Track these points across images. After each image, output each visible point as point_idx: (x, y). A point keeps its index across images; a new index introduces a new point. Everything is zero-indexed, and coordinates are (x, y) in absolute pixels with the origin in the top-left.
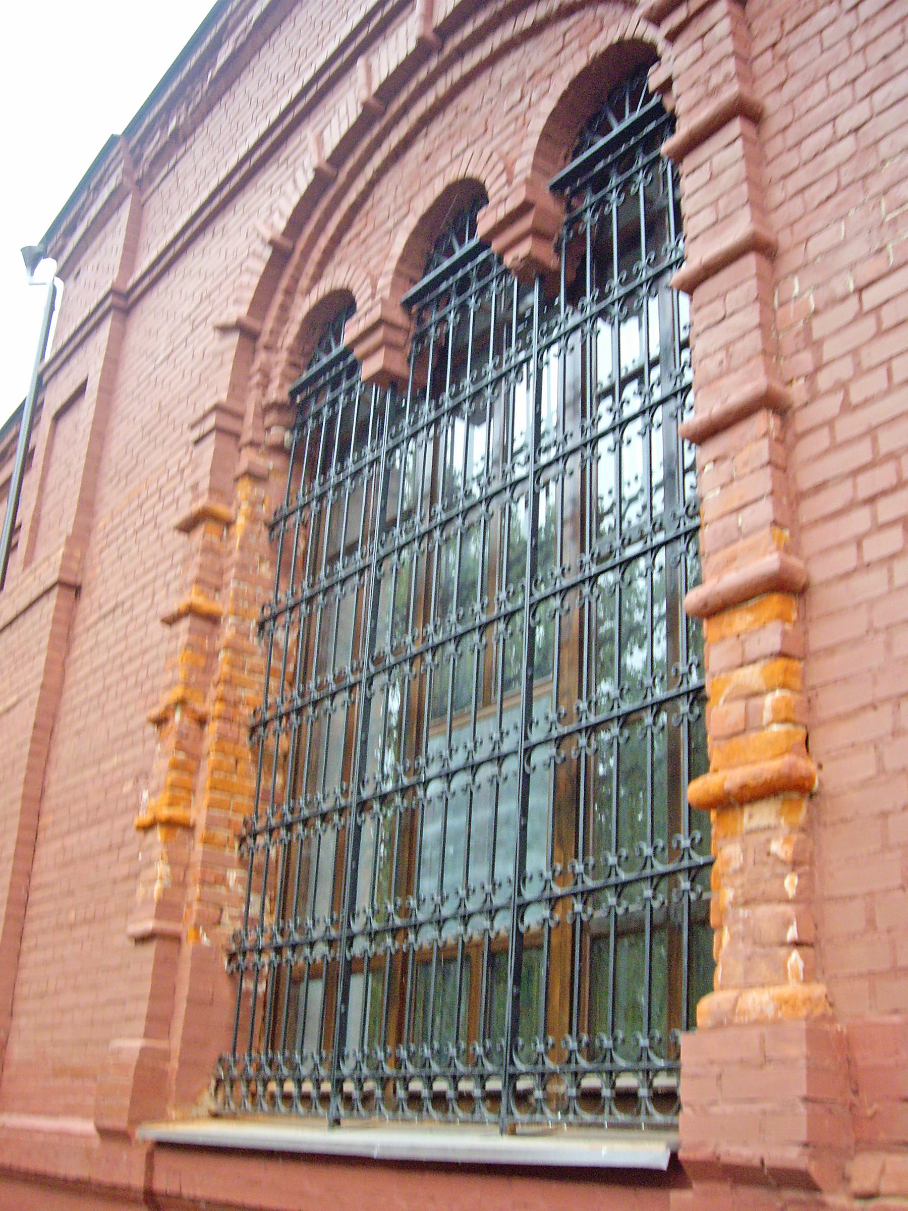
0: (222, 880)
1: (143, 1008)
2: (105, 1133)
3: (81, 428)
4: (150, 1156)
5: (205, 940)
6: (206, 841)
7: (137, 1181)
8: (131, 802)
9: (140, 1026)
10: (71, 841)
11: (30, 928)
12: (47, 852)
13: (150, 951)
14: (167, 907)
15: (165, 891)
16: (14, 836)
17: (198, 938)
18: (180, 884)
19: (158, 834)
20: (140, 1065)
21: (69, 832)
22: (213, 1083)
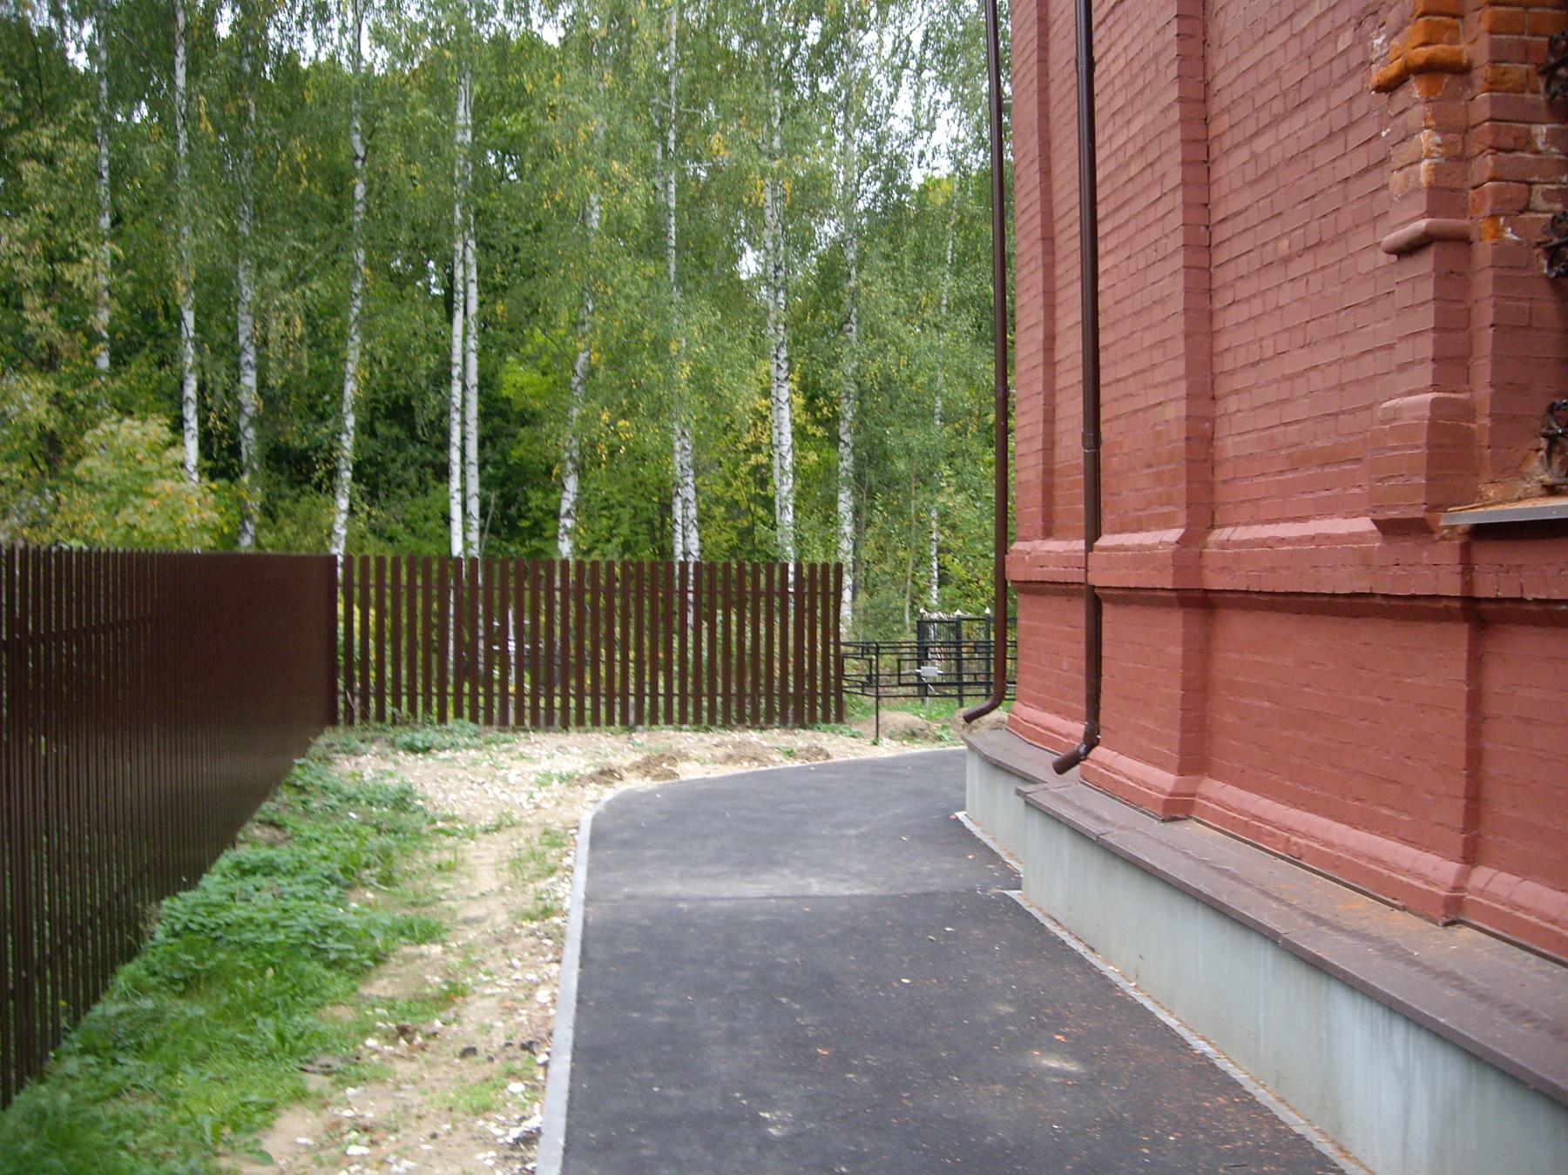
0: (1526, 142)
1: (1426, 346)
2: (1388, 528)
3: (525, 1123)
4: (1465, 550)
5: (1509, 234)
6: (1492, 86)
7: (1451, 585)
8: (1356, 58)
9: (1425, 374)
10: (1260, 145)
11: (1220, 277)
12: (1230, 169)
13: (1425, 263)
14: (1441, 195)
15: (1436, 170)
16: (1177, 156)
17: (1498, 232)
18: (1458, 158)
19: (1415, 89)
20: (1433, 425)
21: (1256, 134)
22: (1544, 443)
